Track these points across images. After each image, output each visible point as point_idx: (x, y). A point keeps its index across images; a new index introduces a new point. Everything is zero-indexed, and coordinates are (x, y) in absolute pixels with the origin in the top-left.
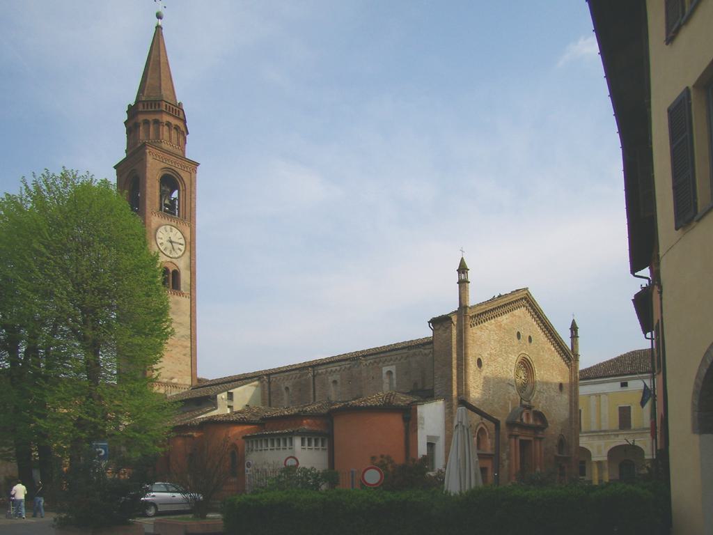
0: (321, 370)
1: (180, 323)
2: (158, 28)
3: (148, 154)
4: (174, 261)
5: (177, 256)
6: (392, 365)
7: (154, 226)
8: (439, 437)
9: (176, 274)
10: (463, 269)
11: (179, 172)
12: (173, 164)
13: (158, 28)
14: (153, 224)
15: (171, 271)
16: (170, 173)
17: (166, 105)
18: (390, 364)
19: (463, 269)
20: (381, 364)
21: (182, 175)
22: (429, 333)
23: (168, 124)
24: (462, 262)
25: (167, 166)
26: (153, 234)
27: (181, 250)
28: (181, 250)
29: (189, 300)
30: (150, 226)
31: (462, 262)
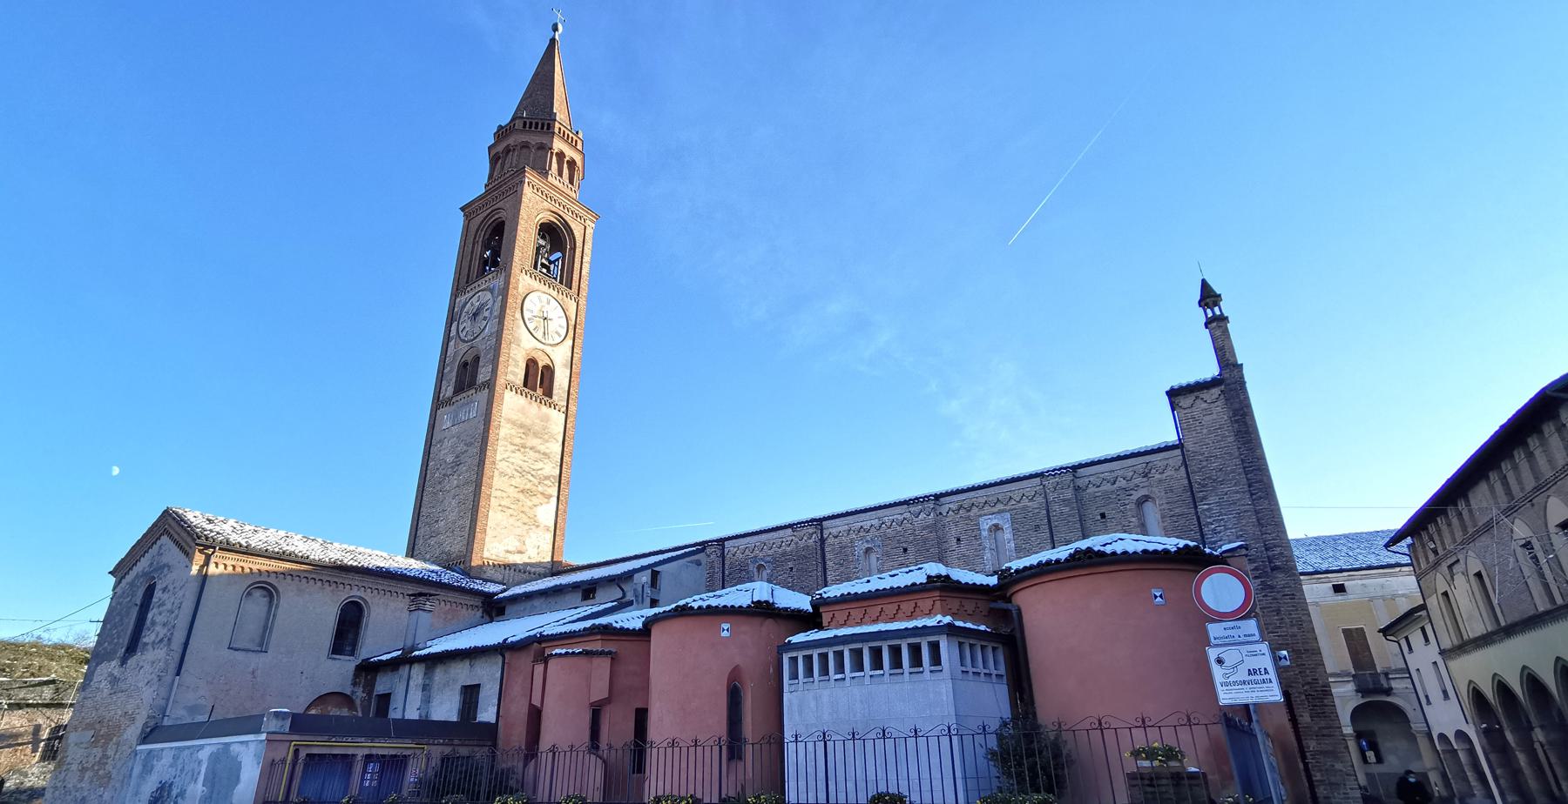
0: (1081, 471)
1: (544, 454)
2: (553, 41)
3: (526, 184)
4: (548, 349)
5: (551, 342)
6: (1000, 512)
7: (522, 290)
8: (889, 646)
9: (549, 371)
10: (1208, 297)
11: (569, 222)
12: (561, 208)
13: (553, 41)
14: (520, 286)
15: (541, 364)
16: (555, 221)
17: (560, 129)
18: (995, 510)
19: (1208, 297)
20: (975, 510)
21: (573, 226)
22: (1163, 430)
23: (561, 155)
24: (1204, 284)
25: (554, 209)
26: (519, 301)
27: (560, 336)
28: (560, 336)
29: (564, 415)
30: (516, 288)
31: (1204, 284)
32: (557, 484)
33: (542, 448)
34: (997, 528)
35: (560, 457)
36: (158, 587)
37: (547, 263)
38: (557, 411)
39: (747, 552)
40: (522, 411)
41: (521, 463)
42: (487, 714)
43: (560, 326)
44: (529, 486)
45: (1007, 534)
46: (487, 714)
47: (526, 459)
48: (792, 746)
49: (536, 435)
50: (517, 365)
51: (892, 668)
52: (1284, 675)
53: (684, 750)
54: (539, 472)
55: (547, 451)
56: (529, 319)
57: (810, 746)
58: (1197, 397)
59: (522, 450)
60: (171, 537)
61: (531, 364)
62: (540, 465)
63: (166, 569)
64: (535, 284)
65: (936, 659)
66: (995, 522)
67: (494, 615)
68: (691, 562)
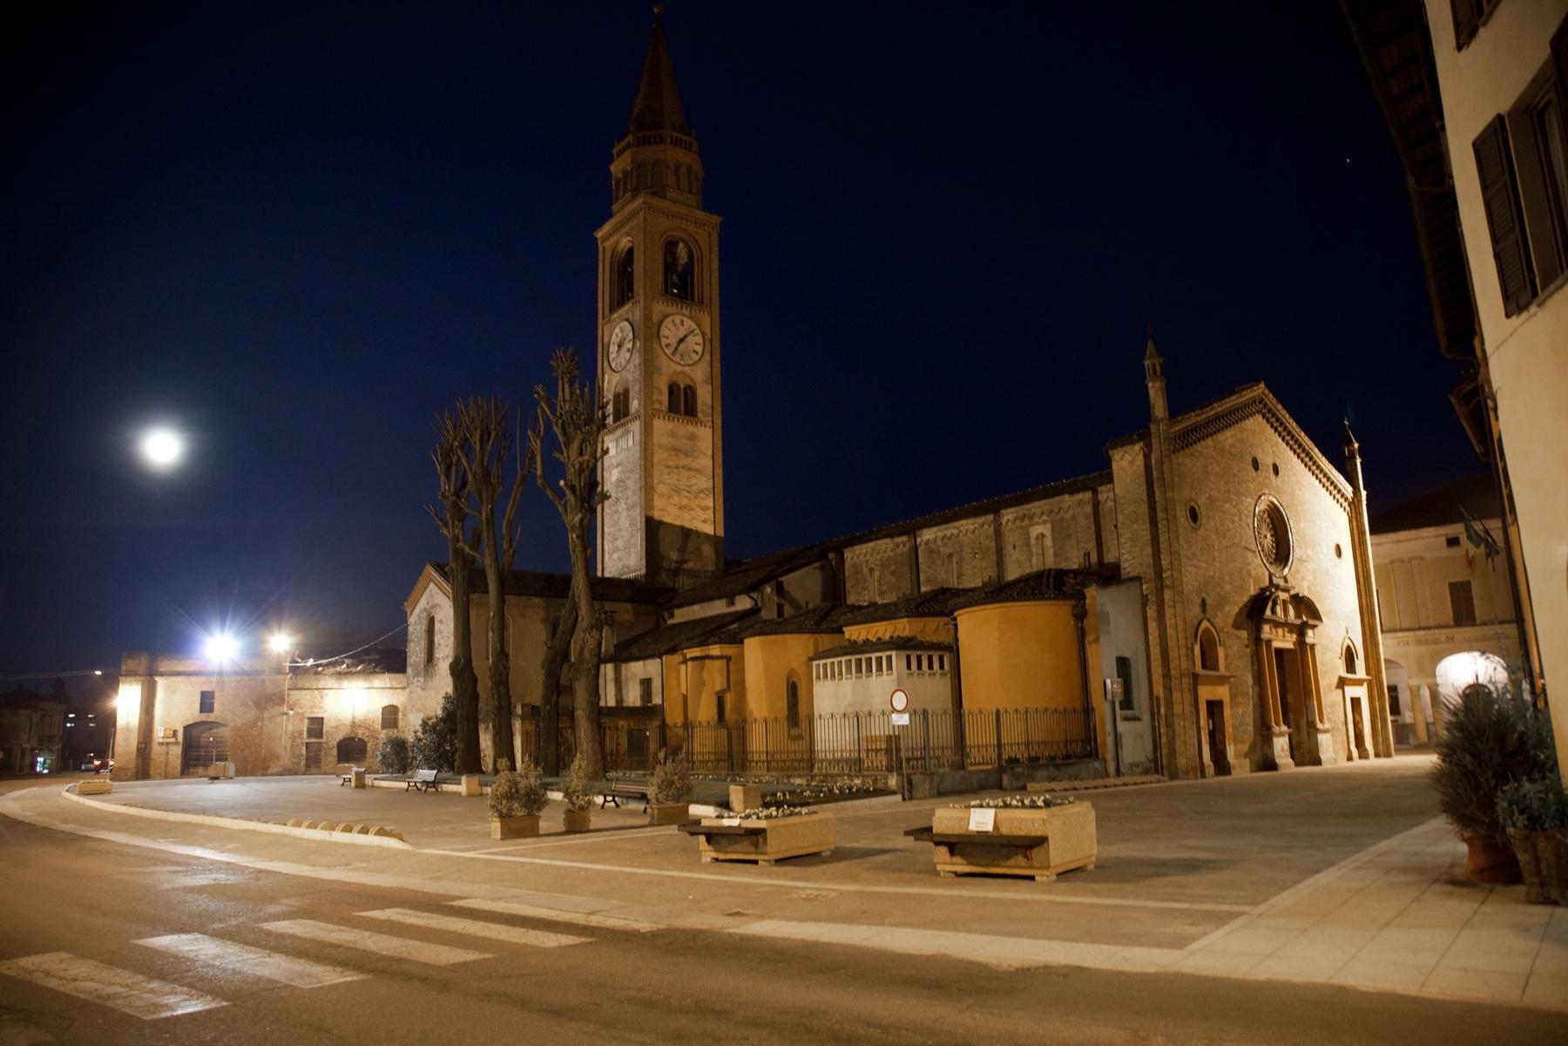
1: (696, 470)
4: (687, 369)
9: (690, 392)
26: (655, 330)
32: (712, 496)
33: (694, 465)
34: (1042, 536)
35: (712, 470)
36: (436, 620)
37: (604, 621)
38: (703, 428)
39: (861, 557)
40: (673, 434)
41: (676, 483)
42: (657, 700)
43: (696, 344)
44: (686, 502)
45: (1048, 542)
46: (657, 700)
47: (680, 478)
48: (967, 717)
49: (687, 455)
50: (660, 393)
51: (857, 673)
52: (140, 776)
53: (877, 718)
54: (694, 488)
55: (698, 467)
56: (666, 346)
57: (851, 719)
58: (1125, 452)
59: (676, 471)
60: (435, 584)
61: (673, 389)
62: (693, 481)
63: (438, 608)
64: (671, 309)
65: (890, 667)
66: (1040, 531)
67: (666, 618)
68: (814, 568)
